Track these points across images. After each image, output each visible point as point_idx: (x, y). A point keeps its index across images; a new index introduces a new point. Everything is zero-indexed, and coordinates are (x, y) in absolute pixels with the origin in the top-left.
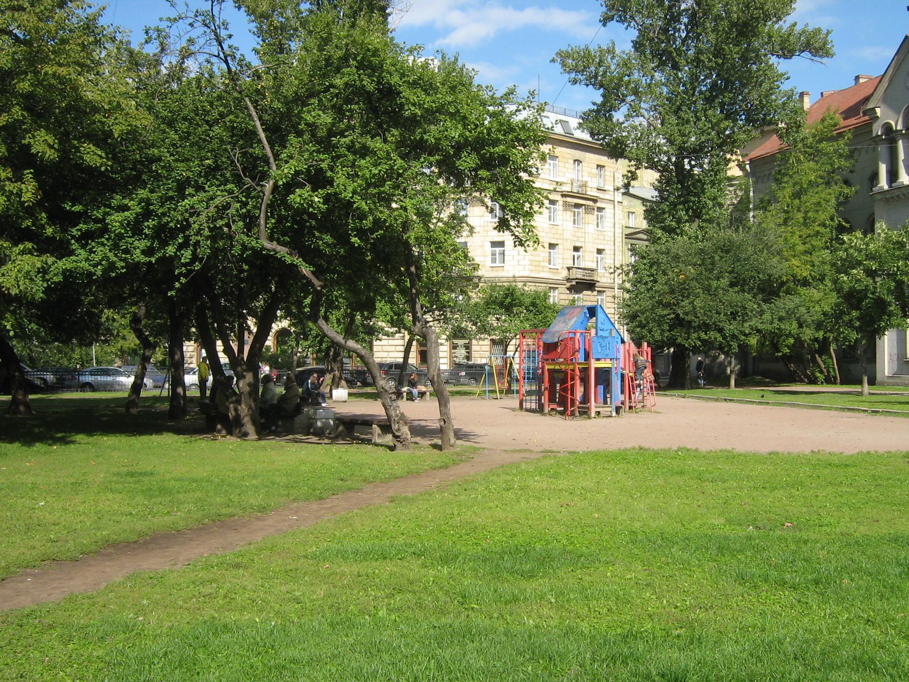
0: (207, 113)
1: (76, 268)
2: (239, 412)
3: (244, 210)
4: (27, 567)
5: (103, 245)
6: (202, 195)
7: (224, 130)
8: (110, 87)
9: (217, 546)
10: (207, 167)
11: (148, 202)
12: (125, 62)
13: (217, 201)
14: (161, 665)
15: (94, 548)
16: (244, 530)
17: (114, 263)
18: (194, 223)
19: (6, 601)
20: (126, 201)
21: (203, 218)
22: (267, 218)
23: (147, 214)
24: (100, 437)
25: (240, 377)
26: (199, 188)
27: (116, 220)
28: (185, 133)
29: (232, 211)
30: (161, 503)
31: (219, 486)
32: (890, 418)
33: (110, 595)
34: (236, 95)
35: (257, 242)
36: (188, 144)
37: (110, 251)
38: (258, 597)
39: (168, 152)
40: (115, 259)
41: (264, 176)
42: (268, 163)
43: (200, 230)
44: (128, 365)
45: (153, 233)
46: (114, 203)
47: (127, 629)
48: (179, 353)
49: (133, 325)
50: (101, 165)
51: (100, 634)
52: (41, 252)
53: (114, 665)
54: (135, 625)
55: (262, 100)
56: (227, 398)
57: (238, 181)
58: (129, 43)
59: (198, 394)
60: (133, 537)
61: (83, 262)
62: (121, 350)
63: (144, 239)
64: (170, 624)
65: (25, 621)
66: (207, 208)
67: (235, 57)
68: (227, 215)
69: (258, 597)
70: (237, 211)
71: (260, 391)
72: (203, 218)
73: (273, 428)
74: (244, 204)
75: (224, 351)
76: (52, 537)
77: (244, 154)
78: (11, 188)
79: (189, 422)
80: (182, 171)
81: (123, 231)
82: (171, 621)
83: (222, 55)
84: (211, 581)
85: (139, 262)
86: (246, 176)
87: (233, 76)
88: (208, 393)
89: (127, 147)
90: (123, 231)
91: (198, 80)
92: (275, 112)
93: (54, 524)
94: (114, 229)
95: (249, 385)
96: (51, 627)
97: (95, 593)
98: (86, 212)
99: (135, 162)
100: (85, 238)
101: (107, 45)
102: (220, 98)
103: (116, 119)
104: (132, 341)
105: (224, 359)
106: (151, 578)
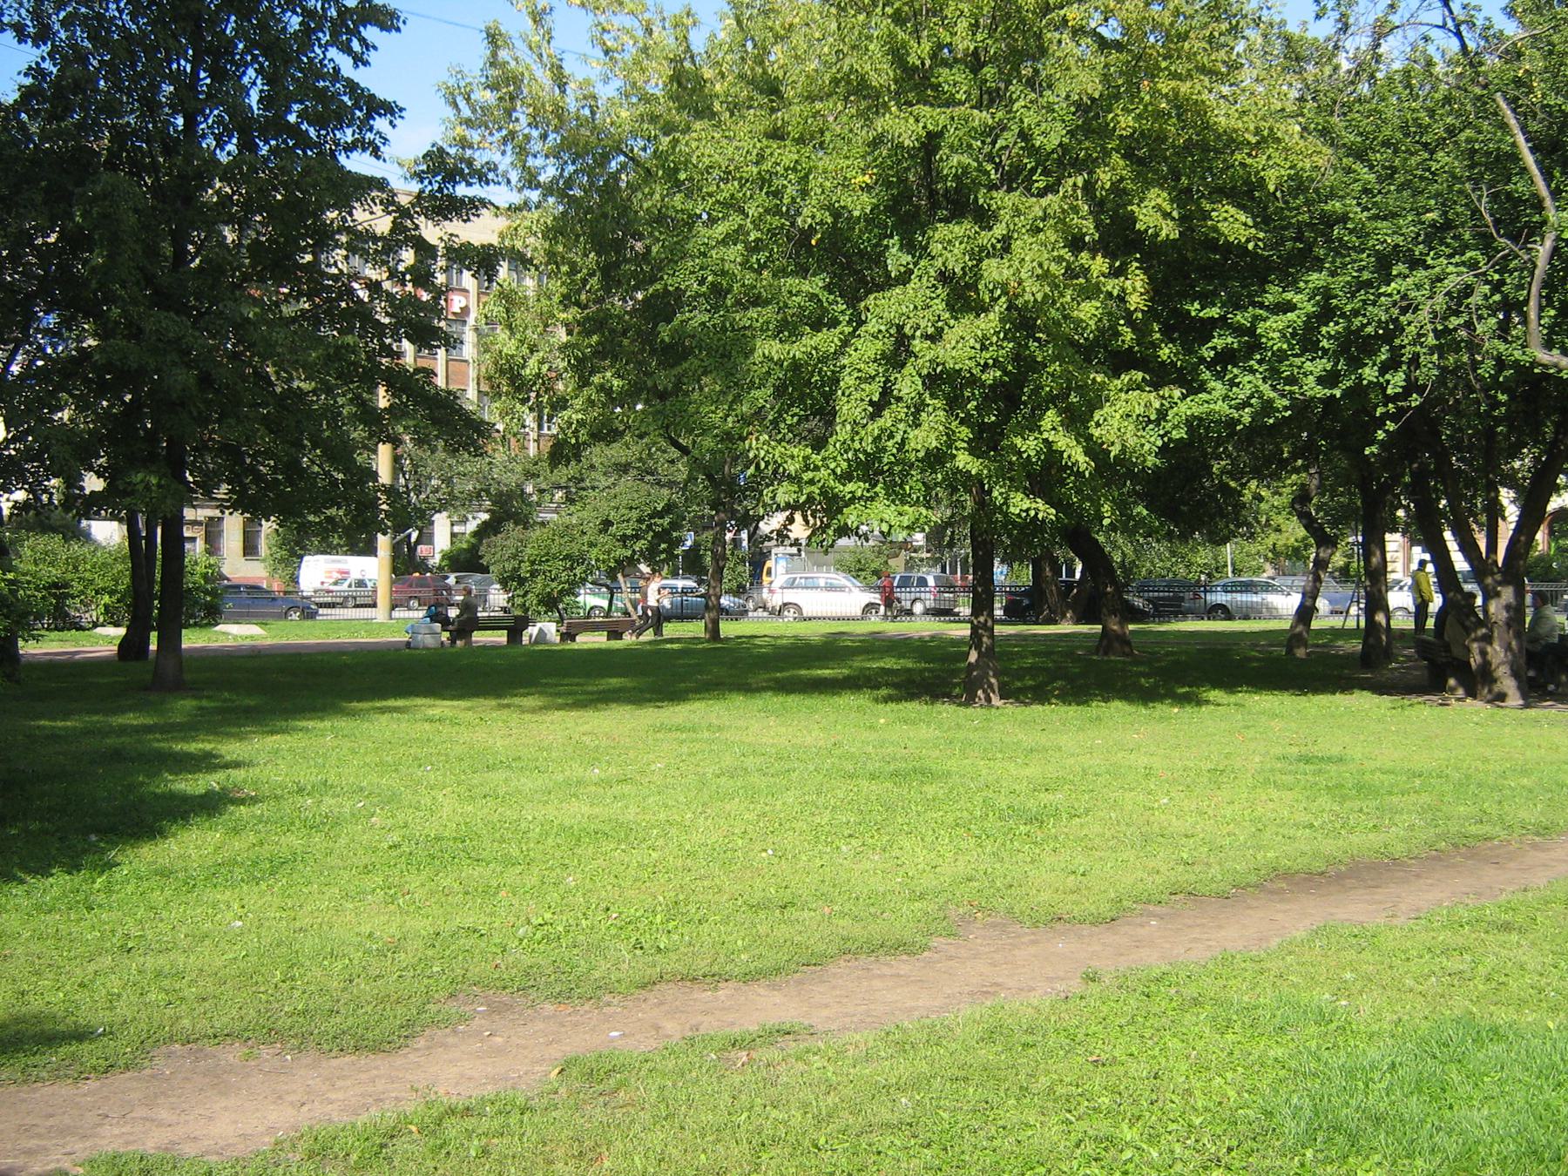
0: (1424, 129)
1: (1208, 414)
2: (1489, 657)
3: (1497, 297)
4: (1149, 902)
5: (1253, 371)
6: (1421, 274)
7: (1456, 158)
8: (1256, 104)
9: (1464, 889)
10: (1429, 226)
11: (1327, 293)
12: (1277, 56)
13: (1450, 283)
14: (1384, 1085)
15: (1253, 879)
16: (1512, 865)
17: (1271, 401)
18: (1409, 324)
19: (1122, 955)
20: (1289, 296)
21: (1424, 315)
22: (1541, 309)
23: (1326, 313)
24: (1247, 695)
25: (1489, 595)
26: (1416, 263)
27: (1273, 328)
28: (1387, 168)
29: (1475, 300)
30: (1361, 810)
31: (1461, 785)
32: (793, 700)
33: (1289, 959)
34: (1478, 91)
35: (1524, 353)
36: (1392, 188)
37: (1264, 380)
38: (1549, 985)
39: (1359, 204)
40: (1273, 395)
41: (1537, 229)
42: (1539, 206)
43: (1420, 335)
44: (1284, 575)
45: (1338, 346)
46: (1269, 299)
47: (1323, 1018)
48: (1378, 553)
49: (1297, 506)
50: (1248, 240)
51: (1277, 1021)
52: (1156, 386)
53: (1304, 1074)
54: (1334, 1013)
55: (1527, 94)
56: (1468, 631)
57: (1485, 243)
58: (1283, 23)
59: (1410, 624)
60: (1318, 865)
61: (1220, 402)
62: (1274, 549)
63: (1321, 358)
64: (1395, 1017)
65: (1153, 988)
66: (1431, 298)
67: (1474, 25)
68: (1467, 306)
69: (1549, 985)
70: (1486, 297)
71: (1528, 620)
72: (1424, 315)
73: (1551, 687)
74: (1497, 287)
75: (1462, 549)
76: (1185, 856)
77: (1494, 197)
78: (1109, 288)
79: (1396, 674)
80: (1386, 235)
81: (1285, 346)
82: (1396, 1013)
83: (1450, 24)
84: (1462, 951)
85: (1313, 398)
86: (1501, 237)
87: (1471, 60)
88: (1430, 623)
89: (1286, 202)
90: (1285, 346)
91: (1407, 73)
92: (1550, 114)
93: (1186, 836)
94: (1270, 343)
95: (1508, 608)
96: (1196, 1002)
97: (1263, 954)
98: (1223, 318)
99: (1300, 227)
100: (1225, 358)
101: (1247, 33)
102: (1448, 100)
103: (1269, 157)
104: (1294, 531)
105: (1460, 563)
106: (1356, 936)
